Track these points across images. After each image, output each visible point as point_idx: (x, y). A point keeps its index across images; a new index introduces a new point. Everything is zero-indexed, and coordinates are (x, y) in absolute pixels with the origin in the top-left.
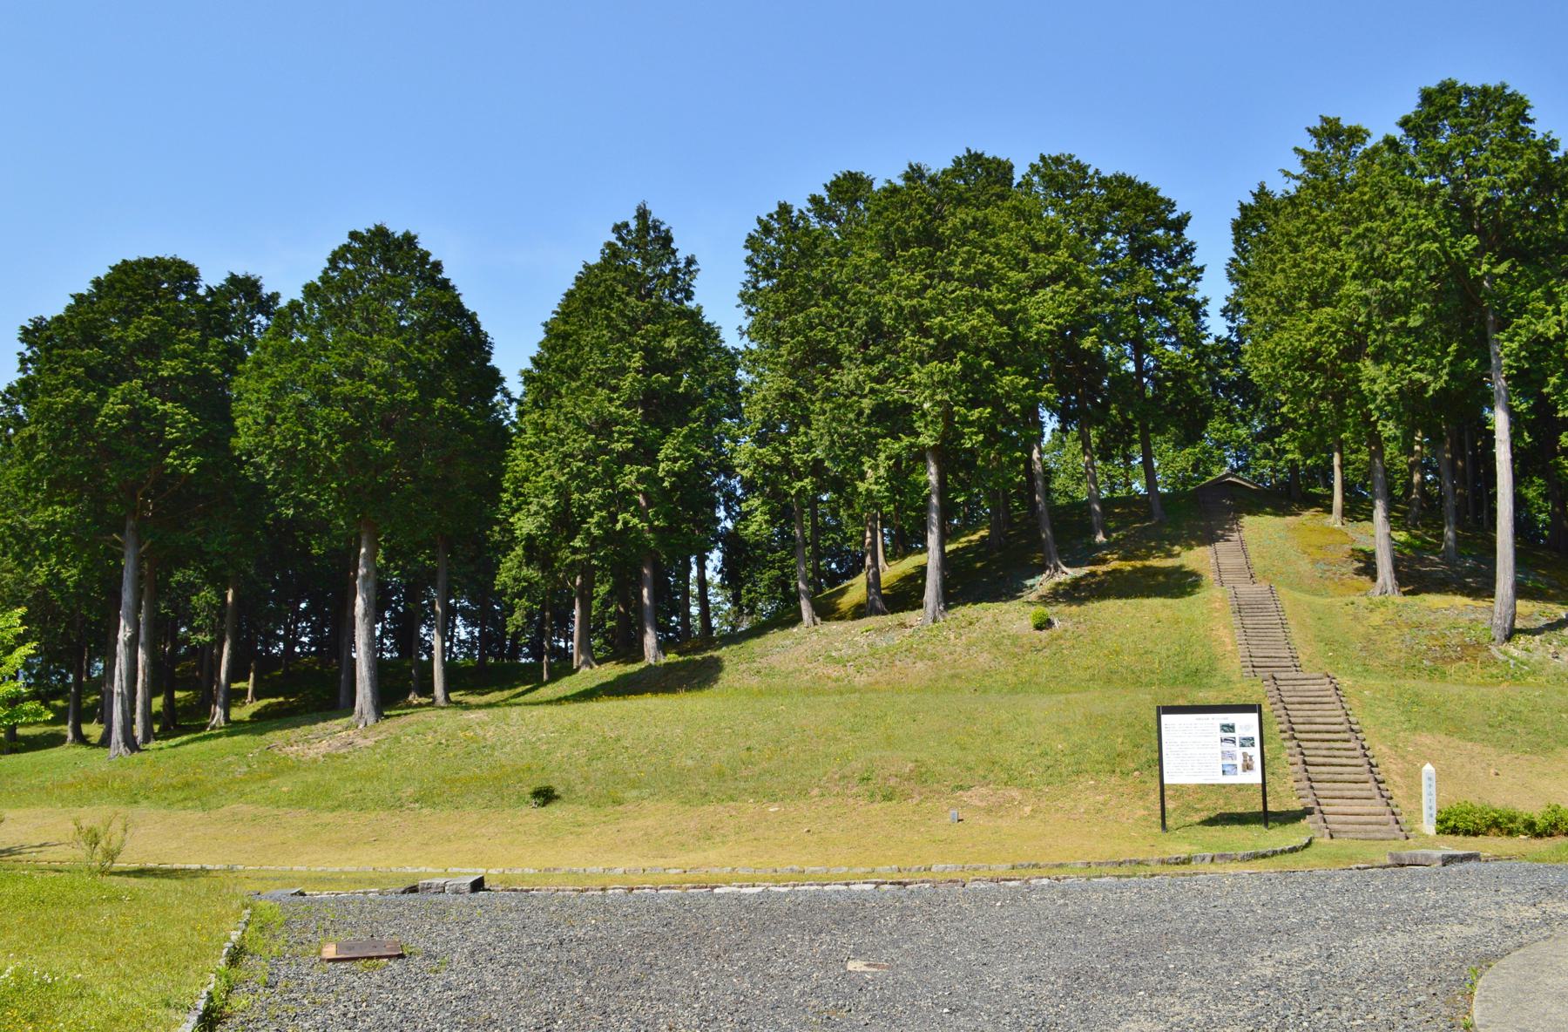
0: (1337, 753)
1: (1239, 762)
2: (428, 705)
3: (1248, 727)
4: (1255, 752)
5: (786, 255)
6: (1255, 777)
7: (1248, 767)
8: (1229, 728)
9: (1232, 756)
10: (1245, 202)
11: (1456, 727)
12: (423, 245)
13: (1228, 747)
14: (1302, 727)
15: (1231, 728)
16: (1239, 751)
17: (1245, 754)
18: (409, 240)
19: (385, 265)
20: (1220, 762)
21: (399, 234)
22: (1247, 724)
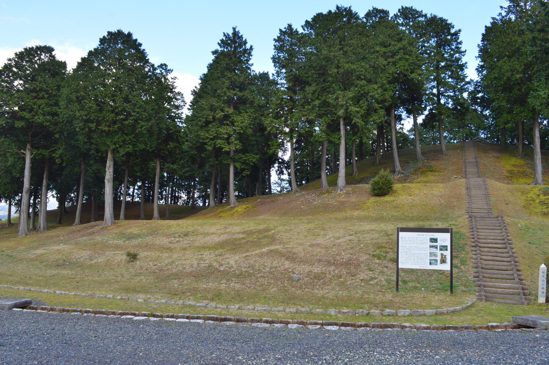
0: (498, 254)
1: (439, 258)
2: (28, 228)
3: (444, 240)
4: (448, 253)
5: (287, 41)
6: (446, 267)
7: (443, 261)
8: (434, 240)
9: (435, 255)
10: (488, 26)
11: (98, 232)
12: (134, 37)
13: (433, 250)
14: (483, 241)
15: (435, 240)
16: (439, 252)
17: (442, 254)
18: (130, 35)
19: (119, 47)
20: (429, 258)
21: (126, 33)
22: (444, 239)
